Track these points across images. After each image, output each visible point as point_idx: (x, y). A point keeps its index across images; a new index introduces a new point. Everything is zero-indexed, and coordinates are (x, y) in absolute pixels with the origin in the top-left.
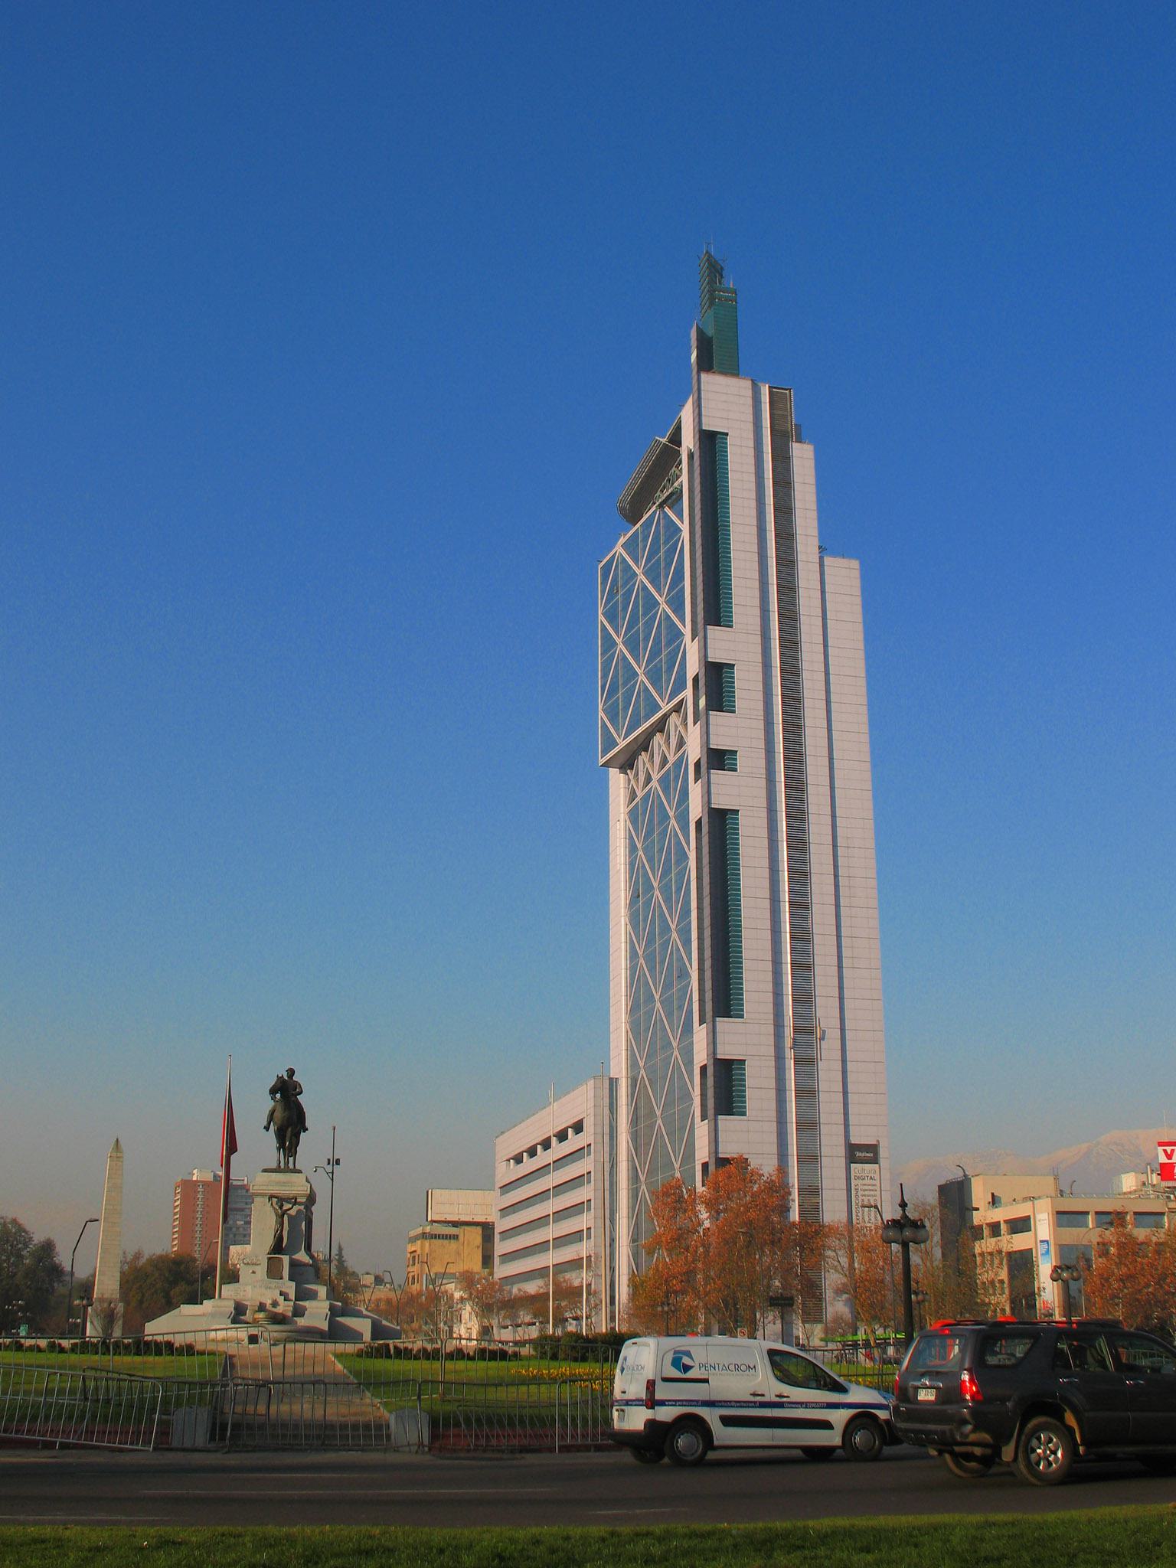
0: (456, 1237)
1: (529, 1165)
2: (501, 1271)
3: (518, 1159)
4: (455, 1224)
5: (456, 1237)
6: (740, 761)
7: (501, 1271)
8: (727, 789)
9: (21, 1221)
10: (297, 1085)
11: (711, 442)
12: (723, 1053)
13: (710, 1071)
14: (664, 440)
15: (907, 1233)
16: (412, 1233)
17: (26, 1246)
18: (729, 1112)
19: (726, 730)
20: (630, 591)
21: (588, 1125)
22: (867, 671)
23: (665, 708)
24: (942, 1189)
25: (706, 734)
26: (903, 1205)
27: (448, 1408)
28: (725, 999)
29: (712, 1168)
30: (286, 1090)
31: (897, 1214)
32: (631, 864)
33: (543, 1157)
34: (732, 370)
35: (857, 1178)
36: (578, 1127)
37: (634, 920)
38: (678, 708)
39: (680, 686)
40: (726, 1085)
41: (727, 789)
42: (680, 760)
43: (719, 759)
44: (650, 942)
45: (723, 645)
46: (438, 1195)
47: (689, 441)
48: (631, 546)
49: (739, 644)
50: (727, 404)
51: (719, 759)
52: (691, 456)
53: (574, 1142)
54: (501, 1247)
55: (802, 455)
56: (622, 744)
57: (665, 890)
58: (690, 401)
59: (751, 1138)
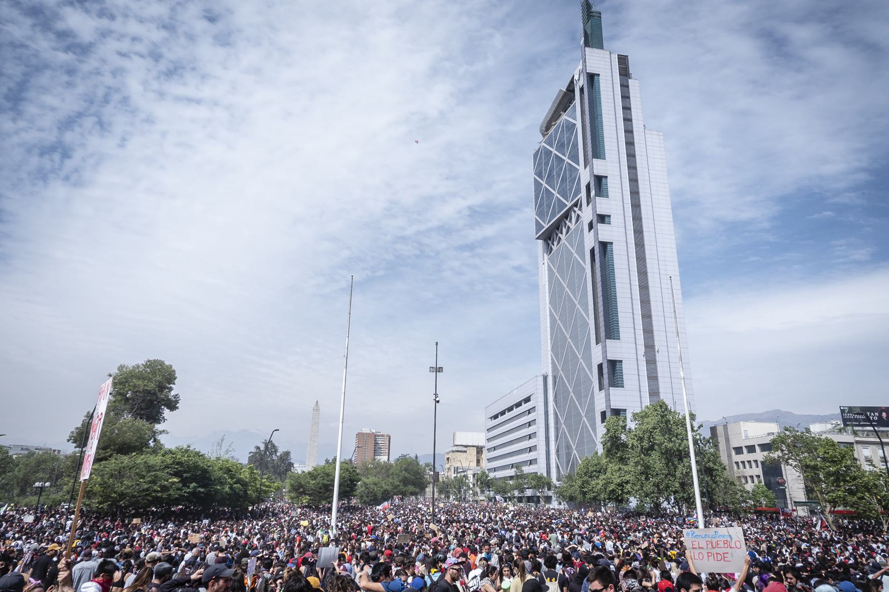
0: (465, 452)
1: (501, 419)
3: (496, 417)
4: (466, 446)
5: (465, 452)
7: (485, 465)
8: (605, 232)
11: (592, 78)
12: (611, 356)
13: (605, 366)
16: (447, 450)
18: (614, 386)
19: (602, 205)
23: (569, 205)
28: (609, 328)
29: (608, 415)
32: (550, 282)
33: (508, 415)
34: (601, 46)
38: (576, 205)
39: (578, 191)
40: (612, 372)
41: (605, 232)
43: (603, 218)
46: (458, 434)
47: (581, 82)
49: (612, 165)
51: (603, 218)
52: (582, 90)
53: (525, 407)
54: (485, 455)
56: (546, 227)
59: (631, 398)
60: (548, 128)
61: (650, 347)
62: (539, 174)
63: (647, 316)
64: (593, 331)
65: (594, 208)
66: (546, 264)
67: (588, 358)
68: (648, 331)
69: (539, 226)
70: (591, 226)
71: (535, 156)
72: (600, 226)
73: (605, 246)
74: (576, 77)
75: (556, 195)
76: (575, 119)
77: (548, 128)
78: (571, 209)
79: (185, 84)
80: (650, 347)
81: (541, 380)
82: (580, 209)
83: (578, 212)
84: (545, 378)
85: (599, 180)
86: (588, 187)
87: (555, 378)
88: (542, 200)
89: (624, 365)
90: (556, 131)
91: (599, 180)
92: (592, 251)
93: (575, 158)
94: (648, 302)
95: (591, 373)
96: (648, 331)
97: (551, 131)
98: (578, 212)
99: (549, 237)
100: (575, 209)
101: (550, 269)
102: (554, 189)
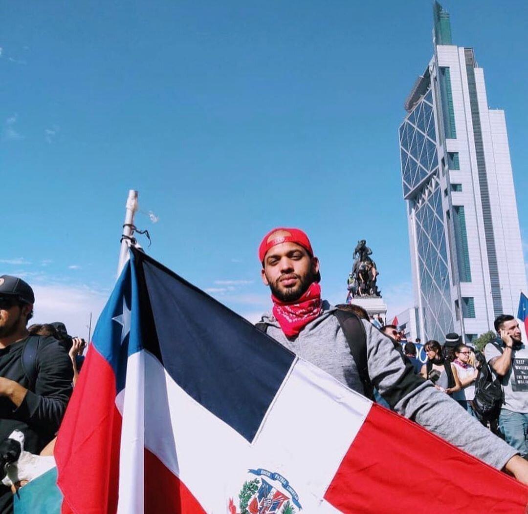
6: (463, 187)
8: (457, 198)
11: (443, 71)
14: (423, 77)
19: (455, 177)
20: (412, 135)
22: (518, 215)
23: (429, 173)
28: (464, 275)
30: (251, 471)
32: (418, 233)
35: (462, 110)
37: (420, 251)
38: (435, 173)
39: (436, 163)
41: (457, 198)
42: (436, 193)
43: (455, 187)
44: (428, 259)
45: (452, 145)
48: (411, 119)
50: (451, 56)
51: (455, 187)
55: (479, 73)
56: (412, 189)
57: (434, 239)
58: (513, 369)
60: (411, 106)
61: (495, 286)
62: (405, 145)
63: (493, 262)
65: (448, 179)
66: (414, 219)
67: (448, 295)
68: (494, 274)
69: (407, 189)
70: (446, 192)
71: (402, 129)
72: (453, 194)
73: (457, 209)
74: (431, 68)
75: (415, 127)
76: (431, 102)
77: (411, 106)
78: (431, 177)
79: (132, 199)
80: (495, 286)
81: (413, 312)
82: (438, 177)
83: (437, 179)
84: (417, 310)
85: (452, 156)
86: (443, 160)
87: (424, 309)
88: (409, 171)
89: (460, 156)
90: (417, 110)
91: (452, 156)
93: (432, 134)
94: (474, 84)
96: (494, 274)
97: (414, 109)
98: (437, 179)
99: (414, 198)
100: (435, 177)
101: (417, 224)
102: (414, 124)
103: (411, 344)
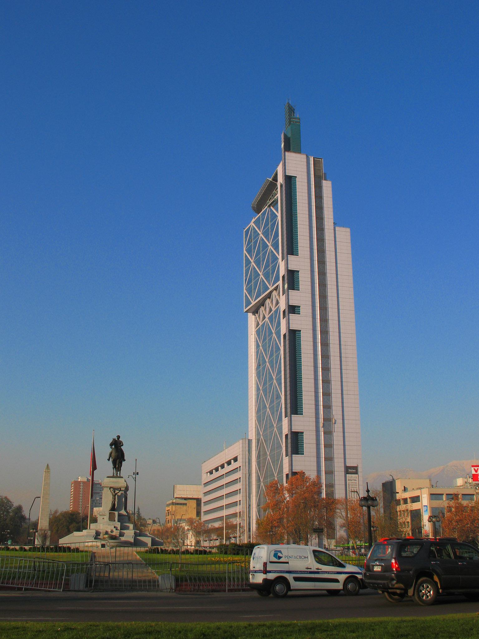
0: (186, 504)
2: (204, 518)
4: (185, 499)
5: (186, 504)
6: (301, 310)
7: (204, 518)
8: (296, 322)
9: (9, 497)
10: (121, 442)
11: (290, 180)
12: (295, 429)
14: (270, 179)
15: (370, 502)
16: (168, 503)
17: (11, 508)
18: (297, 453)
19: (296, 298)
20: (257, 241)
21: (239, 459)
23: (271, 288)
24: (384, 485)
25: (288, 299)
26: (368, 491)
27: (183, 574)
28: (295, 407)
30: (117, 444)
31: (366, 495)
32: (257, 352)
34: (298, 151)
36: (235, 459)
37: (258, 375)
39: (277, 279)
40: (296, 442)
41: (296, 322)
42: (277, 310)
43: (293, 309)
44: (265, 384)
45: (295, 263)
46: (178, 487)
48: (257, 223)
49: (301, 262)
50: (296, 165)
51: (293, 309)
52: (281, 186)
53: (234, 465)
54: (204, 508)
55: (327, 186)
56: (253, 303)
57: (271, 363)
59: (306, 464)
64: (284, 449)
92: (287, 436)
95: (280, 344)
103: (273, 510)
